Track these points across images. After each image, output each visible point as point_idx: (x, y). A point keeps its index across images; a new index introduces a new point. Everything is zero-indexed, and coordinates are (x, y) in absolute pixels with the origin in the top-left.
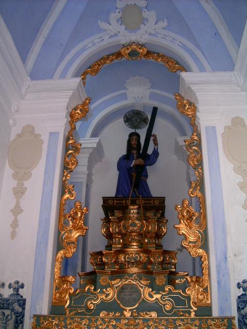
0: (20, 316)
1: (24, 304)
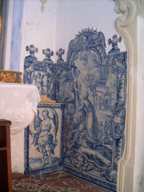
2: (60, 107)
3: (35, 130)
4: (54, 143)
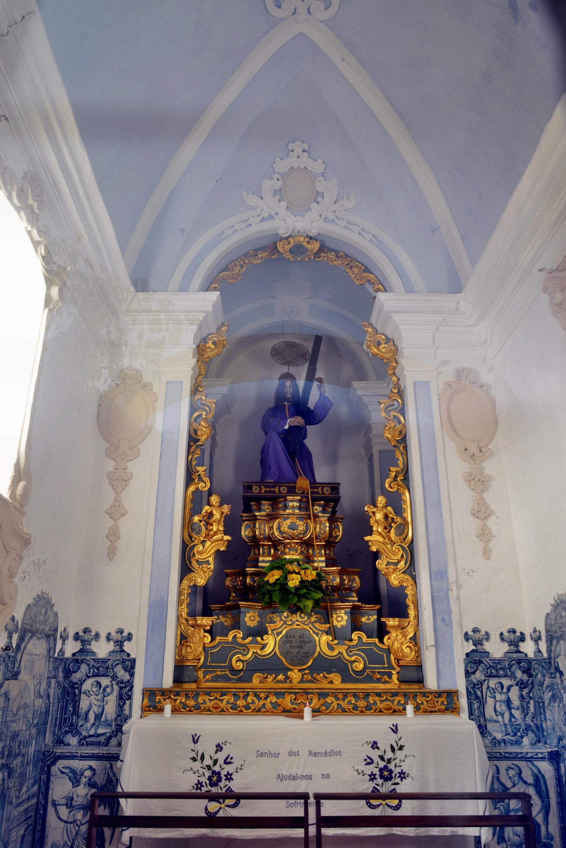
0: (126, 687)
1: (133, 667)
2: (547, 757)
3: (496, 808)
4: (544, 841)
